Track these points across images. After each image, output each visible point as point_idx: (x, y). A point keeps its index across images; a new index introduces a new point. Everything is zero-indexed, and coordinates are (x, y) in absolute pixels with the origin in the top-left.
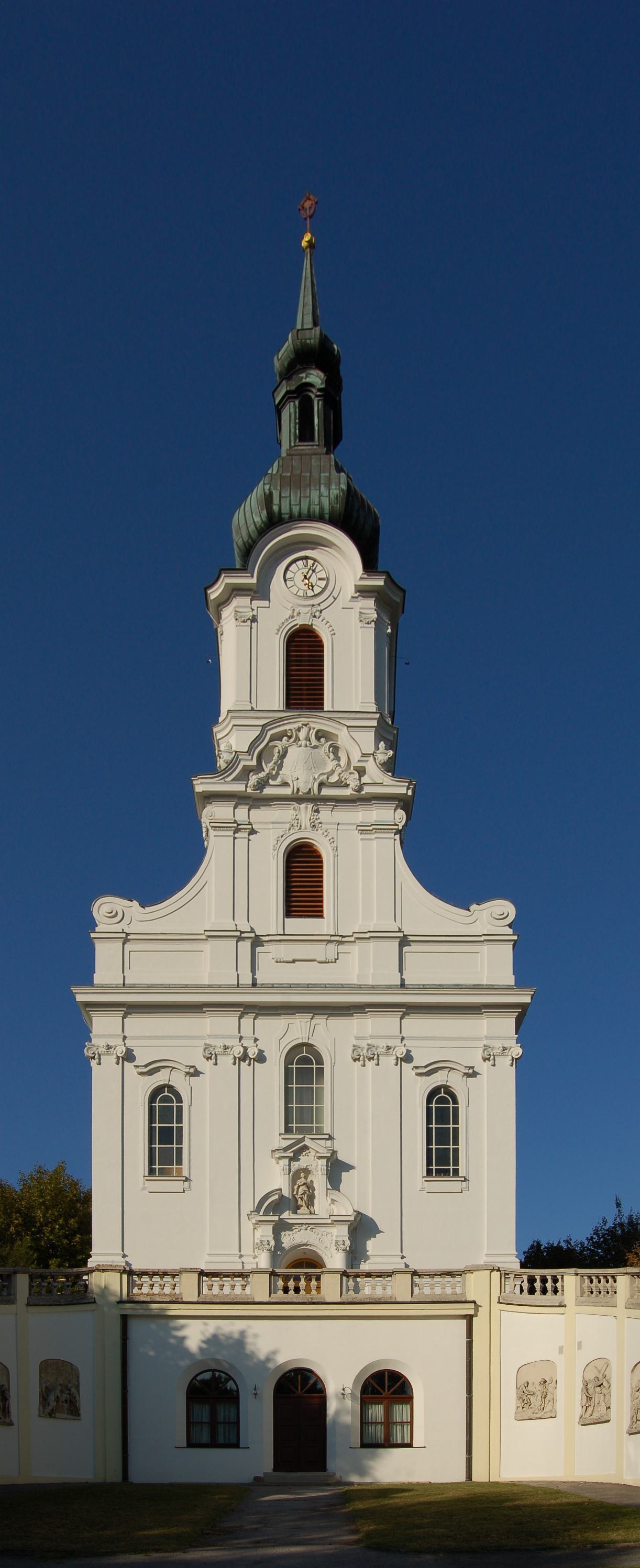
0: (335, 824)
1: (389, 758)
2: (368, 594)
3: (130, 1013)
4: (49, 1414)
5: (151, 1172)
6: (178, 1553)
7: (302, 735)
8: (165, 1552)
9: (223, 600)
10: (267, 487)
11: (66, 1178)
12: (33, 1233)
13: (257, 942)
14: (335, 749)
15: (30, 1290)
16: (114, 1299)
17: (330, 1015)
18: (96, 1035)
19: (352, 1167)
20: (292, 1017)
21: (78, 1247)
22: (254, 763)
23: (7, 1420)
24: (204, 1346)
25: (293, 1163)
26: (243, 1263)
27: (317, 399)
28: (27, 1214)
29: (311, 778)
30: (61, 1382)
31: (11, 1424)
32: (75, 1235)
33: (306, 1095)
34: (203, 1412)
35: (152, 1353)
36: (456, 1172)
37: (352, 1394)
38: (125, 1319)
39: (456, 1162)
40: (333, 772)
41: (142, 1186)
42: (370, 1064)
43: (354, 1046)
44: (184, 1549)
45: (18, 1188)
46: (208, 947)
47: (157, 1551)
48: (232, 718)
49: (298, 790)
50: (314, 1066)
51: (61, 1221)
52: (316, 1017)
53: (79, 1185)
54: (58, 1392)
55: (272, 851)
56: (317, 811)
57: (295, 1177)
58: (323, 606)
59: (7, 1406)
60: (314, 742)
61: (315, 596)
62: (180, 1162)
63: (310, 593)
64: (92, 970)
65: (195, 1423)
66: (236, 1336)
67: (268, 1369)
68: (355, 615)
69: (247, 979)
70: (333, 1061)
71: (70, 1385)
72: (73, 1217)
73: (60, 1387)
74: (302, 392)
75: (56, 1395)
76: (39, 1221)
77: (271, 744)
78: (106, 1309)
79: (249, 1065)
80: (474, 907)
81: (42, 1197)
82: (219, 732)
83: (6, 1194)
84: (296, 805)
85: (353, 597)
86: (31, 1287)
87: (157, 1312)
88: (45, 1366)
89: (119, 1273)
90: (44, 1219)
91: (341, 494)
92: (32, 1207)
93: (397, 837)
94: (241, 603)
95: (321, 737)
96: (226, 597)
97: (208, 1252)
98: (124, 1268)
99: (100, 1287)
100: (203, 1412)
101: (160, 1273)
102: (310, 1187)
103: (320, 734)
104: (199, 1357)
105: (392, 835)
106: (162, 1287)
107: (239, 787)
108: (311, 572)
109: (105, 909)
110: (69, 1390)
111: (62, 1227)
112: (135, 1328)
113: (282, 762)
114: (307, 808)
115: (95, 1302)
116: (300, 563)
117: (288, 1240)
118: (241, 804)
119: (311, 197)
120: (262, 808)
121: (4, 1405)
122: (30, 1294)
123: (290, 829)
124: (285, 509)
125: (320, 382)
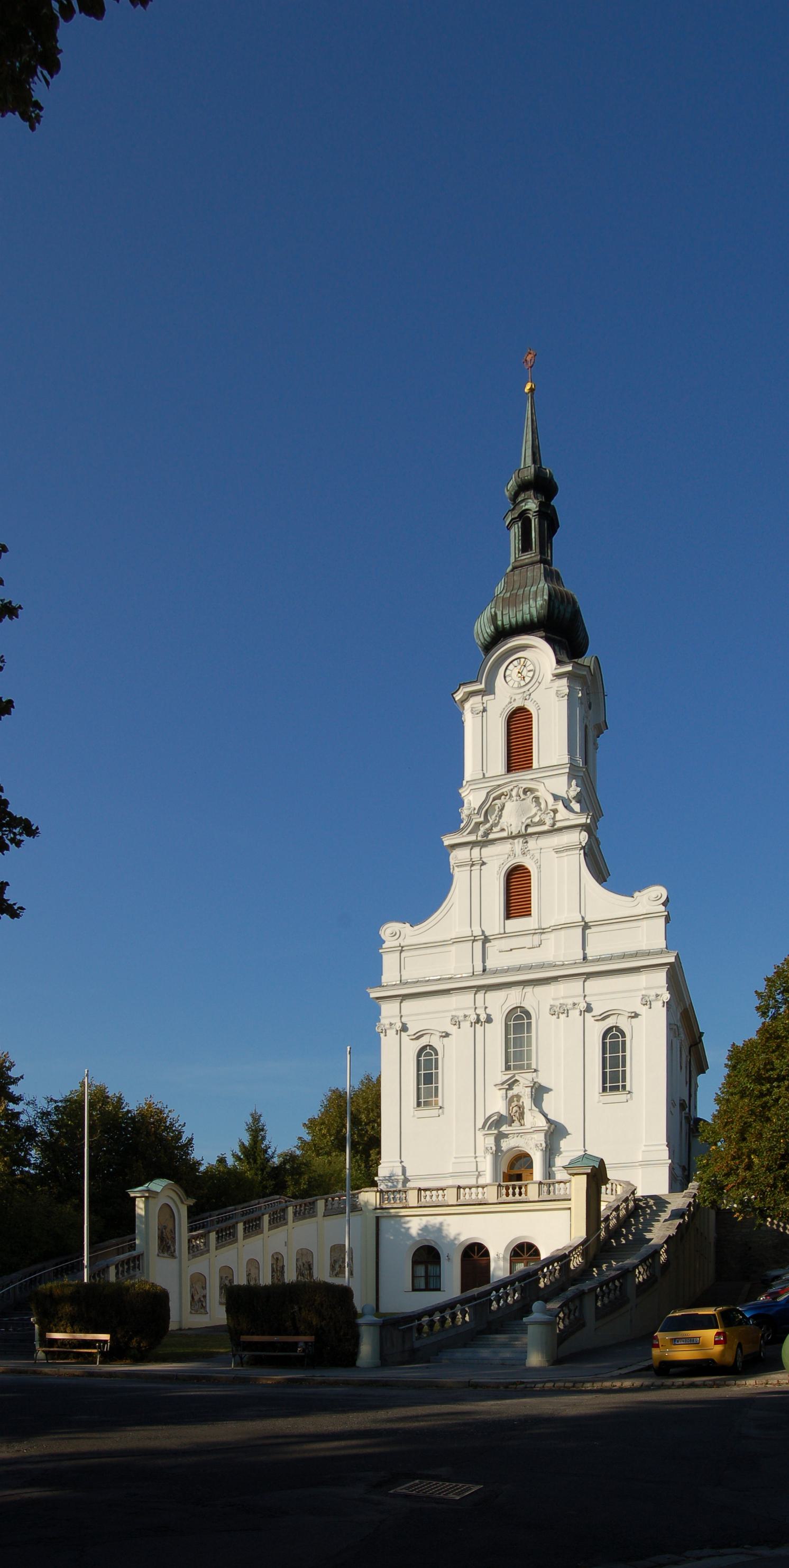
0: (537, 849)
1: (578, 793)
2: (563, 676)
3: (404, 1000)
5: (419, 1104)
7: (514, 793)
9: (464, 699)
10: (493, 610)
13: (486, 940)
14: (537, 799)
16: (371, 1208)
17: (535, 985)
18: (384, 1017)
19: (551, 1090)
20: (510, 989)
22: (482, 819)
24: (420, 1232)
25: (508, 1092)
26: (477, 1162)
27: (534, 517)
29: (520, 823)
33: (519, 1042)
34: (421, 1270)
35: (392, 1238)
36: (624, 1087)
37: (504, 1258)
38: (378, 1218)
39: (624, 1080)
40: (536, 814)
41: (412, 1114)
42: (562, 1017)
43: (551, 1006)
46: (453, 948)
48: (470, 785)
49: (512, 833)
50: (525, 1021)
52: (526, 987)
55: (496, 875)
56: (527, 842)
57: (510, 1101)
58: (531, 690)
60: (523, 797)
61: (527, 684)
62: (436, 1096)
63: (523, 683)
64: (380, 972)
66: (438, 1225)
67: (455, 1244)
68: (553, 692)
69: (479, 968)
70: (538, 1017)
74: (523, 517)
77: (493, 803)
78: (367, 1214)
79: (481, 1025)
80: (636, 894)
82: (464, 792)
84: (511, 840)
85: (552, 680)
91: (544, 603)
93: (582, 852)
94: (475, 701)
95: (527, 792)
96: (466, 697)
97: (454, 1156)
100: (421, 1270)
102: (521, 1108)
103: (526, 790)
104: (418, 1239)
105: (578, 852)
107: (472, 838)
108: (523, 667)
109: (389, 931)
112: (383, 1223)
113: (501, 813)
114: (519, 842)
115: (362, 1210)
116: (515, 663)
117: (505, 1144)
118: (474, 847)
119: (531, 352)
120: (489, 846)
121: (310, 1272)
122: (325, 1210)
123: (508, 858)
124: (506, 621)
125: (535, 506)
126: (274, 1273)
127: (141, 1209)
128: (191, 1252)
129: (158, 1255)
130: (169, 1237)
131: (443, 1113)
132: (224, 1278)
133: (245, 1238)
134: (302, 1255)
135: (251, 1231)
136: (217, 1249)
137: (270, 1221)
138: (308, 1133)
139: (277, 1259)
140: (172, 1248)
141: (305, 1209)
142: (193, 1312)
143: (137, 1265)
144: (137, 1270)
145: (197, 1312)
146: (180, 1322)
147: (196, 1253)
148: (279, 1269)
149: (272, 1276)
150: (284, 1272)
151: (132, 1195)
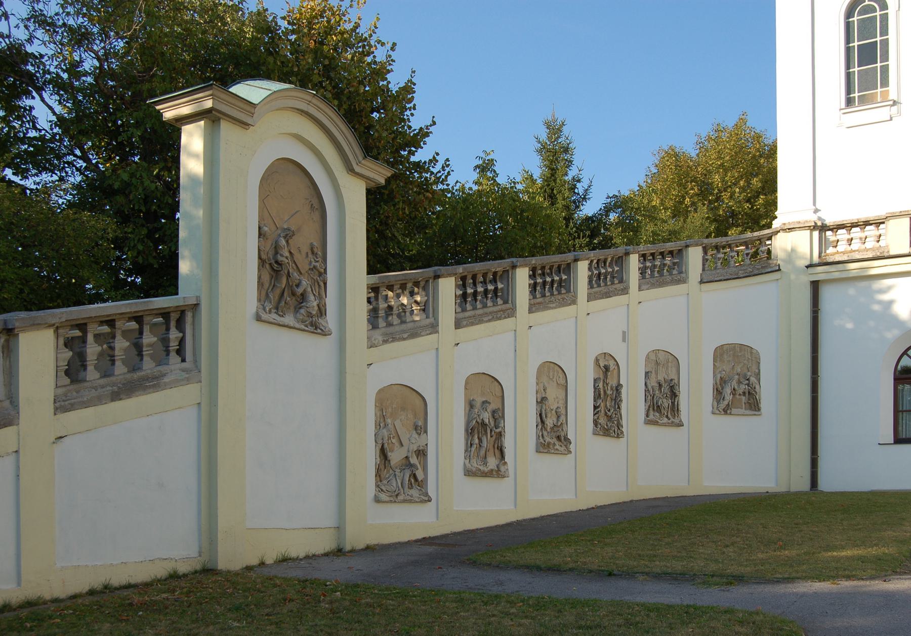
4: (724, 410)
5: (849, 102)
6: (877, 582)
8: (859, 580)
11: (748, 131)
12: (710, 202)
15: (704, 265)
21: (762, 210)
23: (676, 421)
28: (704, 182)
30: (739, 370)
31: (681, 425)
32: (758, 197)
35: (849, 326)
38: (815, 286)
44: (886, 576)
45: (693, 154)
47: (848, 578)
51: (742, 183)
53: (763, 137)
54: (734, 384)
59: (676, 403)
62: (885, 83)
65: (906, 411)
71: (749, 374)
72: (756, 175)
73: (737, 377)
75: (733, 387)
76: (717, 187)
78: (793, 277)
81: (719, 158)
83: (681, 162)
86: (705, 260)
87: (857, 273)
88: (720, 353)
89: (809, 231)
90: (722, 184)
92: (710, 172)
98: (815, 223)
99: (785, 251)
101: (859, 224)
106: (864, 240)
111: (743, 189)
112: (827, 295)
115: (779, 270)
121: (673, 403)
122: (703, 270)
126: (599, 401)
127: (196, 156)
128: (382, 323)
129: (258, 318)
130: (304, 266)
131: (899, 113)
132: (478, 404)
133: (533, 308)
134: (657, 363)
135: (548, 294)
136: (458, 325)
137: (590, 279)
140: (313, 303)
142: (383, 496)
143: (174, 345)
144: (174, 358)
145: (395, 497)
146: (339, 529)
147: (397, 328)
148: (609, 392)
149: (595, 407)
150: (621, 401)
151: (169, 113)
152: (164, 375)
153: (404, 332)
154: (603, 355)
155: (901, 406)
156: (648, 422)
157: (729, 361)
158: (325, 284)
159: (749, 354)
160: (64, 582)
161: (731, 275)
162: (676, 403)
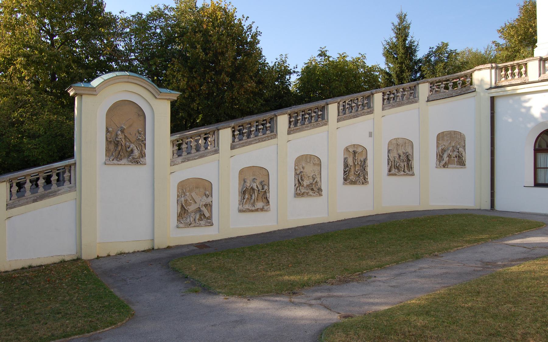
4: (443, 166)
16: (488, 86)
23: (411, 173)
24: (544, 111)
31: (413, 175)
35: (510, 120)
38: (492, 99)
59: (410, 164)
99: (479, 80)
104: (541, 120)
110: (458, 149)
112: (499, 104)
115: (475, 91)
138: (500, 37)
139: (355, 153)
141: (403, 96)
142: (181, 225)
152: (59, 190)
153: (196, 156)
154: (353, 146)
155: (539, 165)
156: (389, 174)
157: (448, 140)
158: (145, 144)
159: (459, 136)
160: (10, 265)
161: (448, 95)
162: (410, 164)
